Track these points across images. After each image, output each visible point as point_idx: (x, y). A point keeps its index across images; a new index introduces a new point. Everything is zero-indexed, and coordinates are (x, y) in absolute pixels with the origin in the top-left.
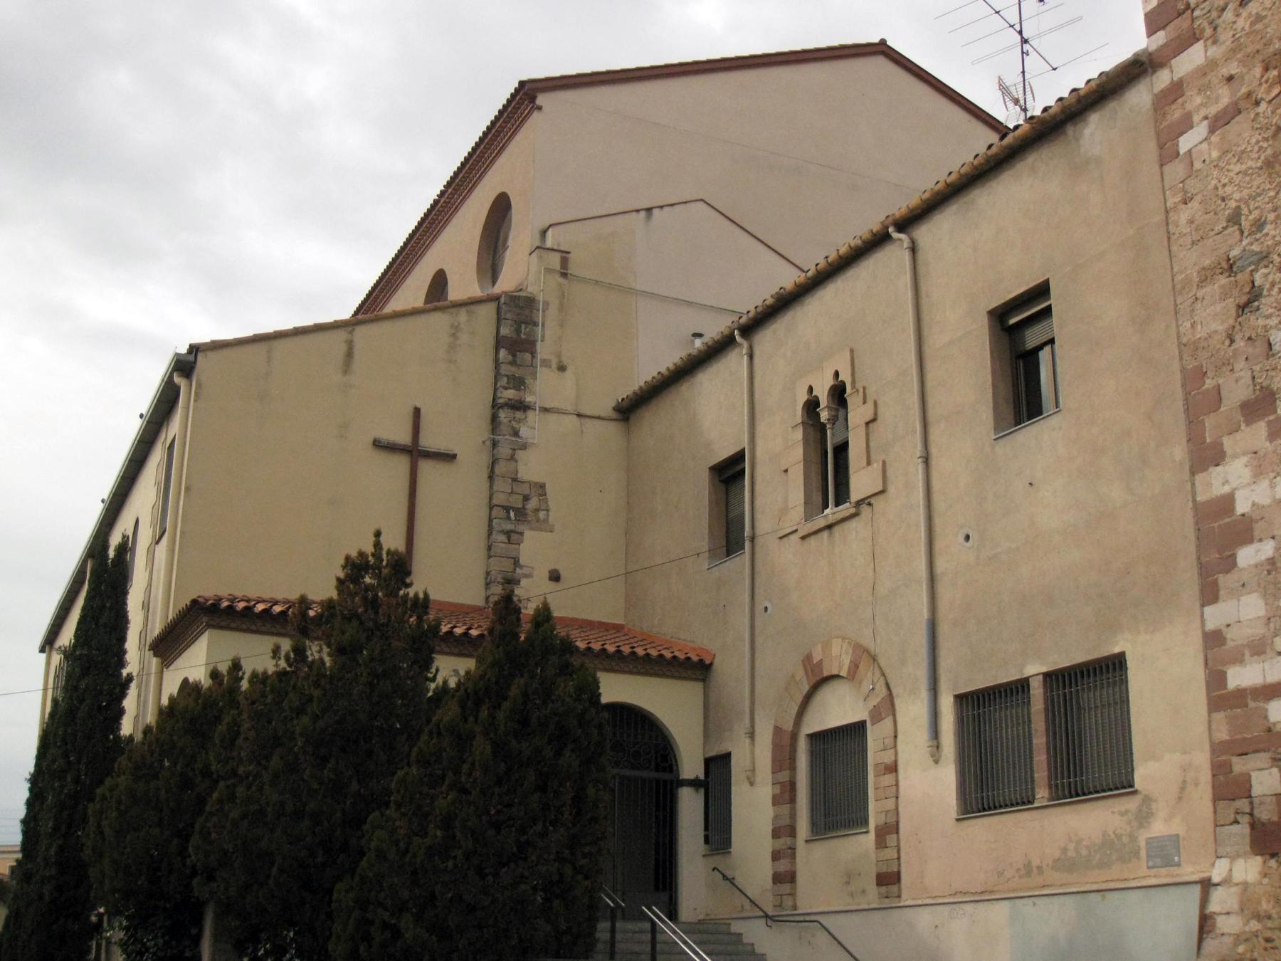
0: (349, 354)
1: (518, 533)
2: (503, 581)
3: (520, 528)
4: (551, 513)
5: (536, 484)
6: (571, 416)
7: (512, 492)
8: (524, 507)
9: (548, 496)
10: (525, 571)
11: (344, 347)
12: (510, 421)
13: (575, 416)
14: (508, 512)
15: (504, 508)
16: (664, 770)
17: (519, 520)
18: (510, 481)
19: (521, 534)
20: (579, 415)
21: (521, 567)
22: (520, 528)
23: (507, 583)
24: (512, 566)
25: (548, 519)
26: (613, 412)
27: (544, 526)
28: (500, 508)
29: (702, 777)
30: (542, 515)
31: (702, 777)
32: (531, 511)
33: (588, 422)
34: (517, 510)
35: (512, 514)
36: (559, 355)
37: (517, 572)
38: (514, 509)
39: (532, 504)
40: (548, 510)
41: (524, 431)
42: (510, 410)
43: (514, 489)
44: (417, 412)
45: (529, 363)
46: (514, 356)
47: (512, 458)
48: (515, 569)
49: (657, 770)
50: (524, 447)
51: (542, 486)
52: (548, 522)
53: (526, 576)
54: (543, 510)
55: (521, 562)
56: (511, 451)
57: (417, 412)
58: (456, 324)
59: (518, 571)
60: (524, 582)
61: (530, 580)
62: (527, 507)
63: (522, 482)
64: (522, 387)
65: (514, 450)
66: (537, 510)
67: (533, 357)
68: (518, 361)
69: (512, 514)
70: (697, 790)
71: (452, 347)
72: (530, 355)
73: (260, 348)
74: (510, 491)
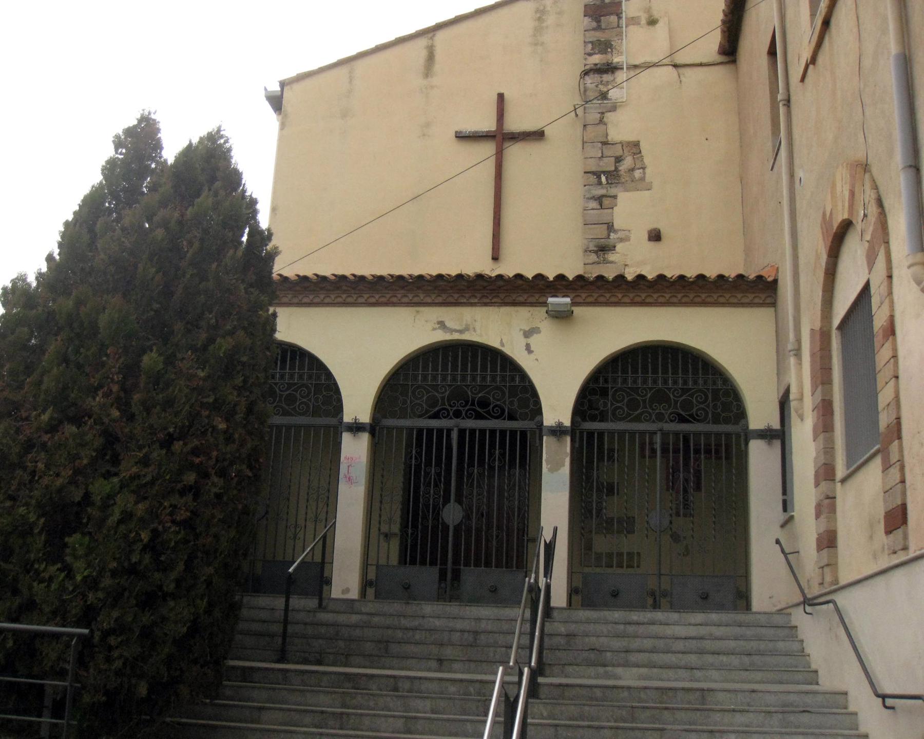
0: (431, 57)
1: (610, 197)
2: (595, 249)
3: (613, 191)
4: (648, 171)
5: (629, 143)
6: (665, 68)
7: (602, 157)
8: (616, 169)
9: (644, 152)
10: (620, 235)
11: (424, 53)
12: (597, 86)
13: (671, 67)
14: (599, 177)
15: (593, 173)
16: (727, 421)
17: (612, 184)
18: (600, 145)
19: (615, 197)
20: (675, 66)
21: (615, 231)
22: (613, 191)
23: (601, 251)
24: (606, 232)
25: (644, 177)
26: (720, 56)
27: (642, 184)
28: (590, 175)
29: (776, 425)
30: (637, 174)
31: (776, 425)
32: (625, 172)
33: (688, 72)
34: (608, 173)
35: (603, 179)
36: (648, 10)
37: (611, 237)
38: (604, 172)
39: (628, 162)
40: (644, 168)
41: (613, 94)
42: (596, 75)
43: (604, 153)
44: (501, 97)
45: (615, 25)
46: (598, 21)
47: (601, 121)
48: (609, 235)
49: (716, 421)
50: (614, 108)
51: (636, 144)
52: (645, 180)
53: (621, 240)
54: (639, 169)
55: (616, 226)
56: (599, 115)
57: (501, 97)
58: (542, 8)
59: (612, 235)
60: (619, 247)
61: (627, 243)
62: (620, 168)
63: (613, 144)
64: (609, 50)
65: (603, 113)
66: (633, 170)
67: (620, 18)
68: (603, 26)
69: (603, 179)
70: (770, 444)
71: (538, 30)
72: (616, 17)
73: (343, 71)
74: (600, 155)
